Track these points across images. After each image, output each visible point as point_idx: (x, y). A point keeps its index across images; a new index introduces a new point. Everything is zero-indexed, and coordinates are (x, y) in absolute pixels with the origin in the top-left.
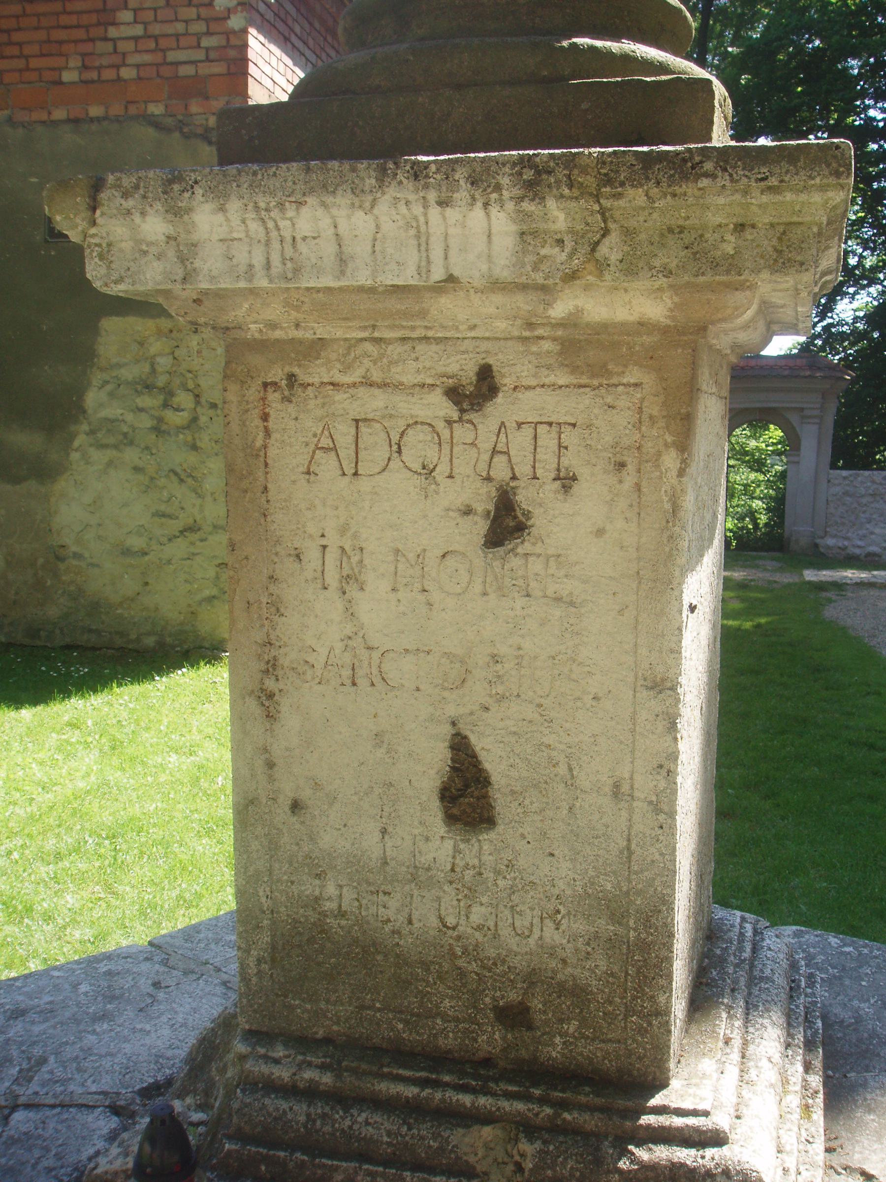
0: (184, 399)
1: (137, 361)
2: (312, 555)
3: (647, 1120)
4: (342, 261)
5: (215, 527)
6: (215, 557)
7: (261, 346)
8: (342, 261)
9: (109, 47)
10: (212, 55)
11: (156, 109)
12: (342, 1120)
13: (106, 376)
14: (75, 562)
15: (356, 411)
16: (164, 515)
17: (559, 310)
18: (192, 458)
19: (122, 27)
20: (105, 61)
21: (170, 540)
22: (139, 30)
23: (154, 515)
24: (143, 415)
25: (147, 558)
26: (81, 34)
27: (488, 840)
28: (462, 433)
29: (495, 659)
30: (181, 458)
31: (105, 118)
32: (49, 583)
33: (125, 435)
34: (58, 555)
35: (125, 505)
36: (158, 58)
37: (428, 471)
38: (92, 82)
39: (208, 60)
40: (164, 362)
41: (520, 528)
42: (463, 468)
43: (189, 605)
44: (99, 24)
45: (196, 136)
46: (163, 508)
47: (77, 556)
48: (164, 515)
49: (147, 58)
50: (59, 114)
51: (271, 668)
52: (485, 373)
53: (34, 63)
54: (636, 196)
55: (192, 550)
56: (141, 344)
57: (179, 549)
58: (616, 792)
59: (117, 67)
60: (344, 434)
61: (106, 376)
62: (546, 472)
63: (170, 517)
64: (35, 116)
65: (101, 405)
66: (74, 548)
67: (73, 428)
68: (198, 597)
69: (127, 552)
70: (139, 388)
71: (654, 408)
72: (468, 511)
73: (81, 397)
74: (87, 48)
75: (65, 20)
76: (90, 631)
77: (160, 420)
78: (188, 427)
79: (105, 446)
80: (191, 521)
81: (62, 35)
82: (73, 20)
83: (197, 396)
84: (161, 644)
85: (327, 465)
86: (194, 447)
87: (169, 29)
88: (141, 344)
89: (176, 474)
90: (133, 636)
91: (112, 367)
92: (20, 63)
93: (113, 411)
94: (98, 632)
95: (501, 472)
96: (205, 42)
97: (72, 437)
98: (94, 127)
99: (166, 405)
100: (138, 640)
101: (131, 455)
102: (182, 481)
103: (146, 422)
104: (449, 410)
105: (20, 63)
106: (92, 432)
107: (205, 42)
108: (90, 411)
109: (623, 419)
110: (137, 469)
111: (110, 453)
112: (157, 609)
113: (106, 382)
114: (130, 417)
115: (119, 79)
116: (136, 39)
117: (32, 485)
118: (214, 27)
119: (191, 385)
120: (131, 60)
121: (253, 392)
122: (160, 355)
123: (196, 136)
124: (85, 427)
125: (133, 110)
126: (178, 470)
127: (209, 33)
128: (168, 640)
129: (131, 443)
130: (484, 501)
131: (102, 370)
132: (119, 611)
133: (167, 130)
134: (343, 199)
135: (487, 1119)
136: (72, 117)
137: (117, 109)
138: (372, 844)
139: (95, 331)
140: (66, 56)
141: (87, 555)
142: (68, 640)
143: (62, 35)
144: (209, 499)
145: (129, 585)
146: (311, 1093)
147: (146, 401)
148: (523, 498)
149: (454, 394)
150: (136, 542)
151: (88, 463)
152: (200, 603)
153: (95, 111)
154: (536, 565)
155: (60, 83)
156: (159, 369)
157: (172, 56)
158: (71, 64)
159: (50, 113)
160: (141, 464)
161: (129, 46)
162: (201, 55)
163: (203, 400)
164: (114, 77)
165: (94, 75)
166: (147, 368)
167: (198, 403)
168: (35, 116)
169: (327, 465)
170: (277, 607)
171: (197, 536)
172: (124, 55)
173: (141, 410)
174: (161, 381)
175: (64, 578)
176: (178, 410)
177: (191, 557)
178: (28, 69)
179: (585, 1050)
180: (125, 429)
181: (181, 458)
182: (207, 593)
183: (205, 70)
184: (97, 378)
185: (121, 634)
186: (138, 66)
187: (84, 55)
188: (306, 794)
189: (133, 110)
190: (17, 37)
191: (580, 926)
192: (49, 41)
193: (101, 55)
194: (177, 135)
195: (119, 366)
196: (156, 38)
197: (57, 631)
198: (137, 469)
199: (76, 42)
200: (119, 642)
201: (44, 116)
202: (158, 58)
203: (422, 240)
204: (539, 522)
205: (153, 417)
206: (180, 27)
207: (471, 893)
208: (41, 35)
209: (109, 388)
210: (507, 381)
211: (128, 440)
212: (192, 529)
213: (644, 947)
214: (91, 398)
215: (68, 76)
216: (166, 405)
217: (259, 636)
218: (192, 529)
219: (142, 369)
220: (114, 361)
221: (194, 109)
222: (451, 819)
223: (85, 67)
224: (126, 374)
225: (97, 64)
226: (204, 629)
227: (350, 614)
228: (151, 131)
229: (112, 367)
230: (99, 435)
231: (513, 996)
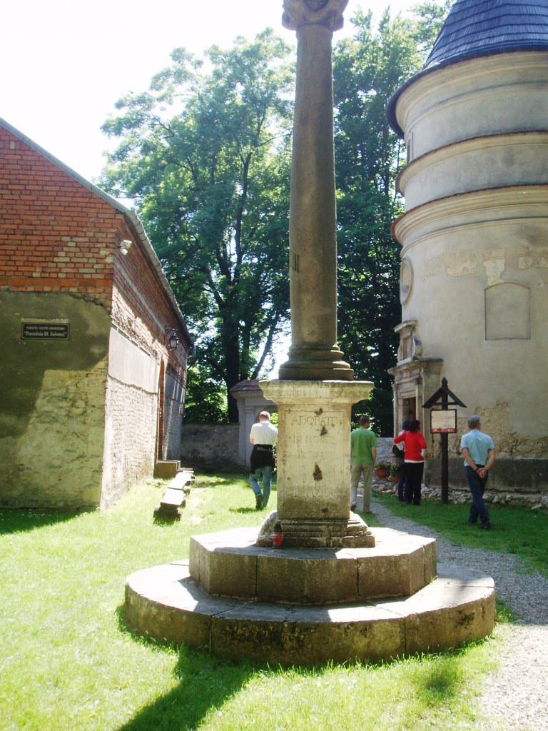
0: (81, 404)
1: (60, 388)
2: (293, 437)
3: (348, 526)
4: (305, 394)
5: (92, 455)
6: (92, 468)
7: (285, 405)
8: (305, 394)
9: (54, 265)
10: (98, 271)
11: (73, 290)
12: (301, 527)
13: (45, 394)
14: (27, 471)
15: (300, 415)
16: (69, 451)
17: (333, 401)
18: (83, 427)
19: (61, 258)
20: (53, 270)
21: (72, 461)
22: (67, 260)
23: (66, 451)
24: (62, 410)
25: (61, 469)
26: (42, 259)
27: (321, 481)
28: (317, 418)
29: (322, 453)
30: (78, 427)
31: (51, 292)
32: (14, 480)
33: (54, 418)
34: (20, 468)
35: (53, 447)
36: (76, 271)
37: (312, 424)
38: (46, 278)
39: (96, 273)
40: (73, 389)
41: (326, 433)
42: (317, 423)
43: (80, 488)
44: (50, 256)
45: (90, 301)
46: (70, 448)
47: (28, 468)
48: (69, 451)
49: (70, 270)
50: (31, 289)
51: (285, 456)
52: (321, 410)
53: (20, 269)
54: (347, 388)
55: (82, 465)
56: (63, 381)
57: (76, 465)
58: (341, 472)
59: (58, 273)
60: (298, 418)
61: (45, 394)
62: (330, 424)
63: (73, 451)
64: (20, 289)
65: (44, 406)
66: (27, 465)
67: (30, 415)
68: (84, 485)
69: (52, 467)
70: (61, 398)
71: (346, 415)
72: (318, 430)
73: (34, 402)
74: (45, 264)
75: (35, 253)
76: (33, 501)
77: (69, 412)
78: (82, 414)
79: (44, 422)
80: (82, 453)
81: (35, 259)
82: (39, 254)
83: (86, 402)
84: (66, 505)
85: (295, 423)
86: (84, 423)
87: (81, 260)
88: (63, 381)
89: (76, 434)
90: (53, 502)
91: (49, 390)
92: (15, 268)
93: (49, 408)
94: (37, 501)
95: (323, 424)
96: (96, 266)
97: (30, 418)
98: (46, 295)
99: (72, 406)
100: (56, 504)
101: (56, 426)
102: (78, 437)
103: (63, 412)
104: (315, 415)
105: (15, 268)
106: (38, 417)
107: (96, 266)
108: (38, 408)
109: (341, 416)
110: (58, 432)
111: (46, 425)
112: (65, 491)
113: (46, 396)
114: (56, 410)
115: (58, 277)
116: (66, 263)
117: (10, 438)
118: (99, 261)
119: (84, 398)
120: (64, 270)
121: (283, 412)
122: (71, 386)
123: (90, 301)
124: (36, 415)
125: (63, 290)
126: (77, 432)
127: (97, 263)
128: (69, 503)
129: (56, 421)
130: (320, 428)
131: (44, 391)
132: (47, 492)
133: (79, 298)
134: (307, 386)
135: (323, 524)
136: (36, 290)
137: (56, 289)
138: (302, 483)
139: (42, 375)
140: (35, 267)
141: (33, 468)
142: (22, 505)
143: (35, 259)
144: (90, 444)
145: (53, 480)
146: (294, 524)
147: (64, 404)
148: (327, 428)
149: (316, 412)
150: (57, 463)
151: (36, 430)
152: (84, 487)
153: (47, 289)
154: (329, 438)
155: (32, 277)
156: (70, 391)
157: (81, 271)
158: (37, 270)
159: (26, 288)
160: (60, 430)
161: (64, 265)
162: (94, 271)
163: (89, 404)
164: (56, 276)
165: (47, 275)
166: (64, 390)
167: (87, 405)
168: (20, 289)
169: (295, 423)
170: (286, 446)
171: (84, 460)
172: (61, 268)
173: (62, 408)
174: (71, 396)
175: (22, 478)
176: (78, 408)
177: (81, 468)
178: (17, 271)
179: (337, 515)
180: (53, 415)
181: (78, 427)
182: (88, 483)
183: (95, 276)
184: (42, 394)
185: (47, 501)
186: (66, 273)
187: (43, 267)
188: (290, 476)
189: (63, 290)
190: (13, 258)
191: (336, 494)
192: (28, 261)
193: (50, 268)
194: (82, 300)
195: (52, 390)
196: (75, 263)
197: (17, 502)
198: (58, 432)
199: (40, 262)
200: (46, 505)
201: (23, 289)
202: (76, 271)
203: (316, 392)
204: (329, 431)
205: (67, 411)
206: (85, 260)
207: (318, 491)
208: (25, 258)
209: (47, 398)
210: (324, 410)
211: (55, 420)
212: (82, 456)
213: (346, 497)
214: (39, 403)
215: (34, 275)
216: (72, 406)
217: (283, 451)
218: (82, 456)
219: (62, 392)
220: (50, 387)
221: (90, 291)
222: (315, 479)
223: (43, 272)
224: (56, 393)
225: (49, 271)
226: (86, 497)
227: (299, 446)
228: (71, 298)
229: (49, 390)
230: (42, 418)
231: (325, 507)
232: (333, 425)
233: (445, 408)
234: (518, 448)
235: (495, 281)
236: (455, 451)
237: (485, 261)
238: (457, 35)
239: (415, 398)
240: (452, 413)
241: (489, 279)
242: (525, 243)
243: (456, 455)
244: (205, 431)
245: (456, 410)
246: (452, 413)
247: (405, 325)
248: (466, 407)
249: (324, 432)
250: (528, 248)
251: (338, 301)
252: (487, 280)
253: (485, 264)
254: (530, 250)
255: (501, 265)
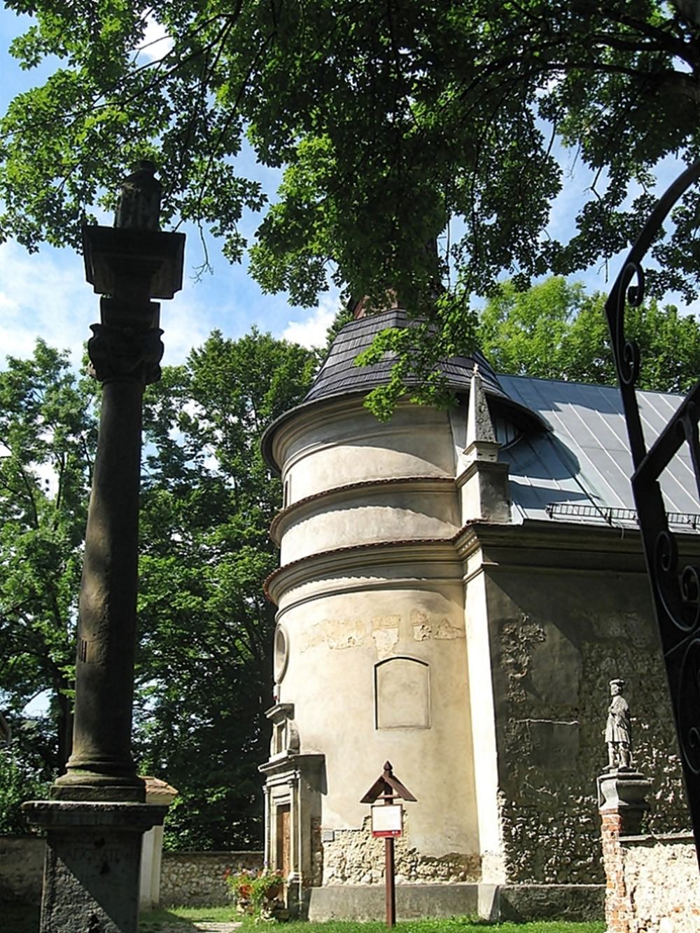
52: (103, 840)
232: (118, 861)
233: (389, 801)
234: (418, 869)
235: (387, 655)
236: (340, 875)
237: (374, 630)
238: (346, 356)
239: (289, 804)
240: (396, 810)
241: (379, 653)
242: (423, 610)
243: (340, 880)
244: (17, 849)
245: (401, 805)
246: (396, 810)
247: (279, 709)
248: (416, 801)
249: (105, 870)
250: (424, 616)
251: (73, 714)
252: (377, 655)
253: (374, 634)
254: (428, 617)
255: (393, 633)
